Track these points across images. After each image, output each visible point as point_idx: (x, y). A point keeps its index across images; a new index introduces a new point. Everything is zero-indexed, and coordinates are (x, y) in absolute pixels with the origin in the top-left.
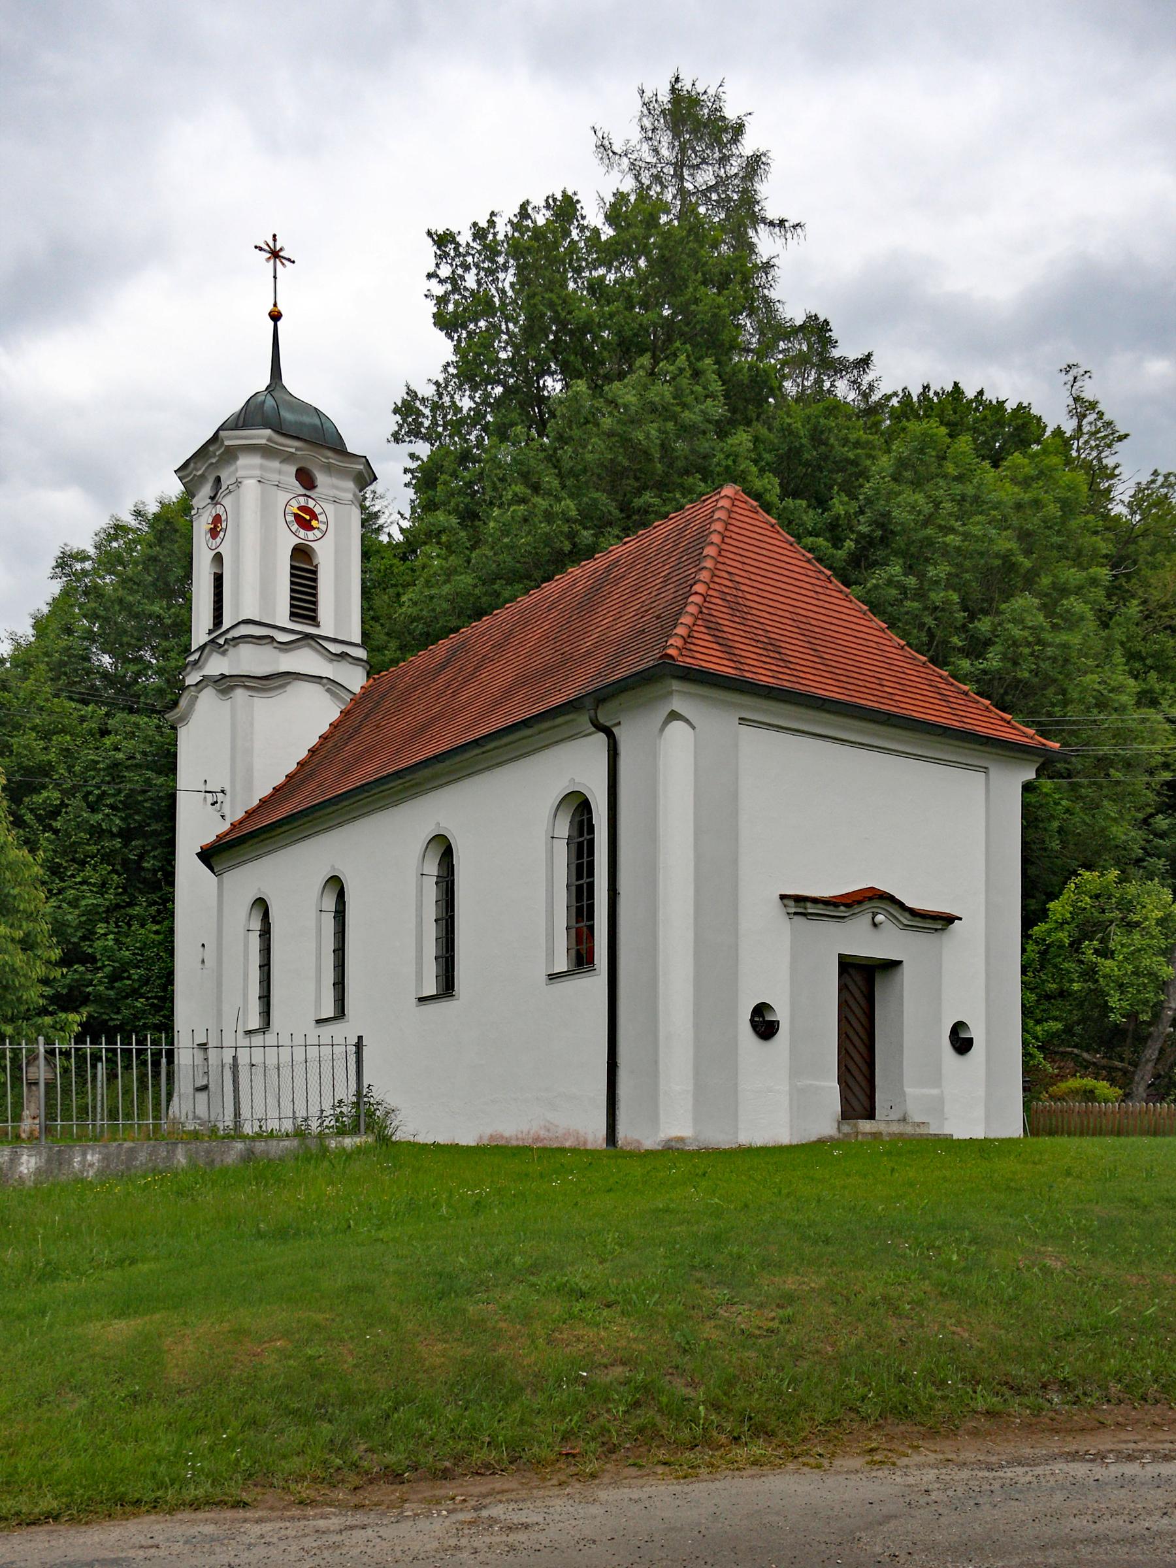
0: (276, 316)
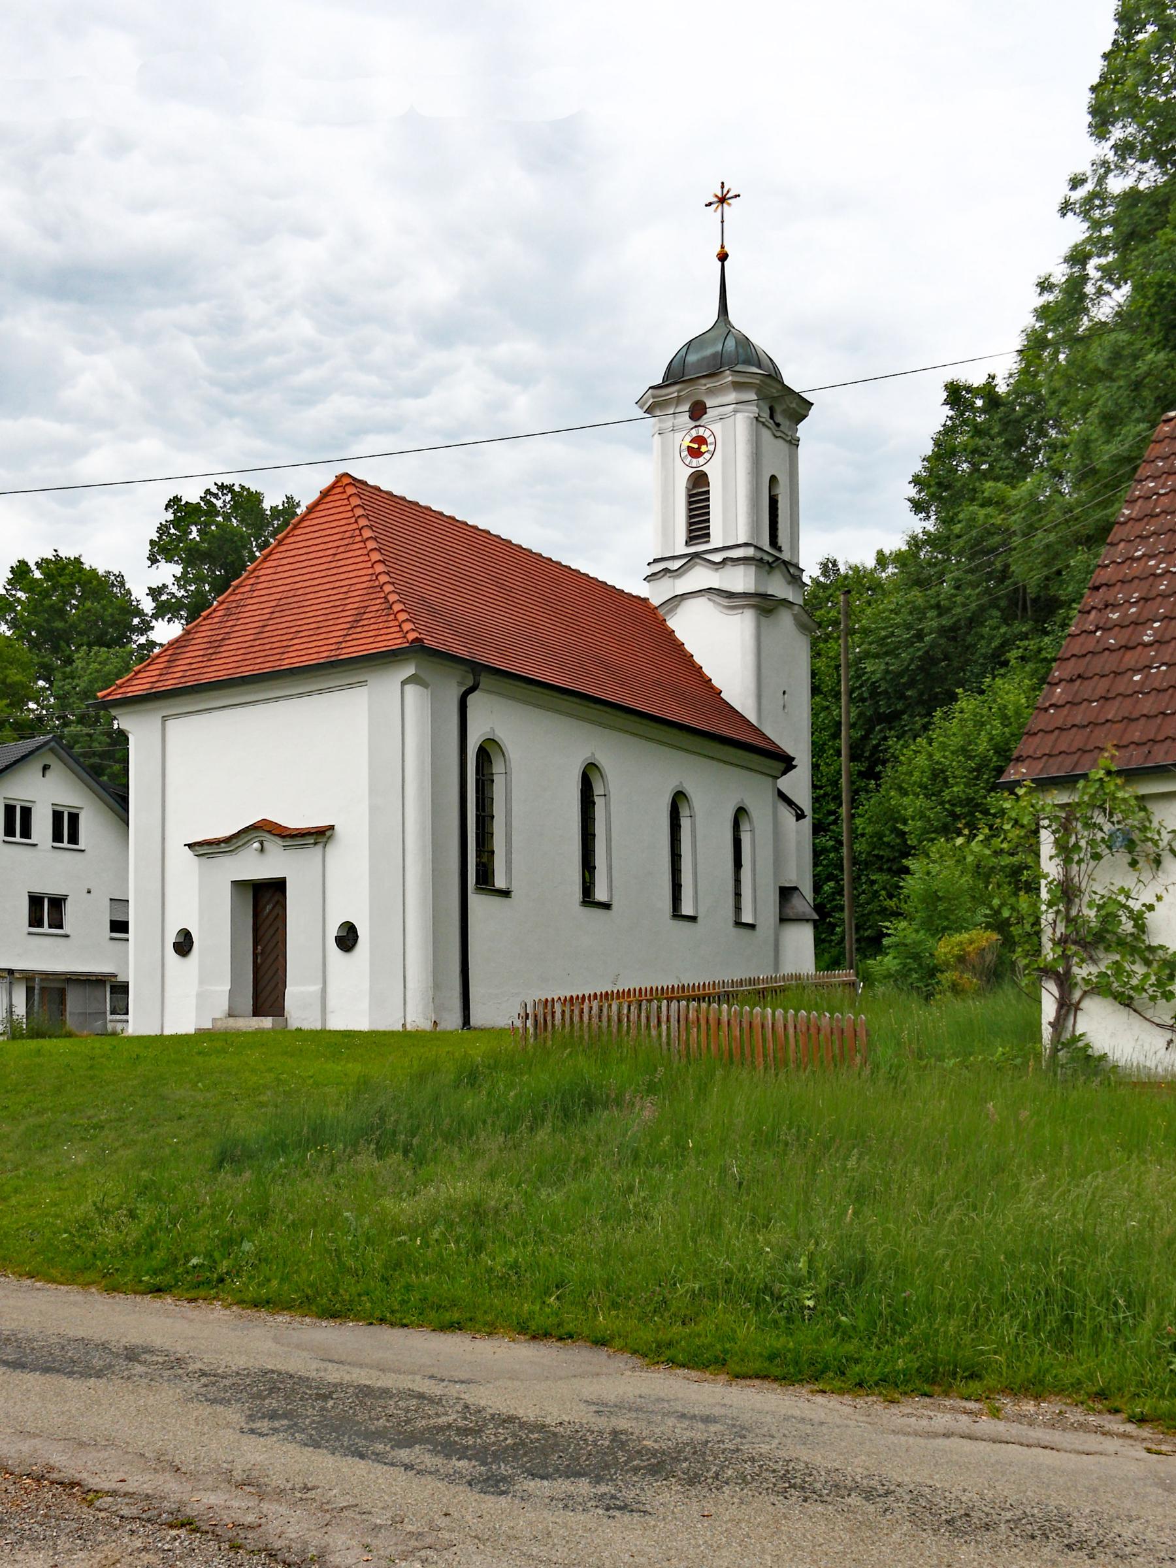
0: (723, 257)
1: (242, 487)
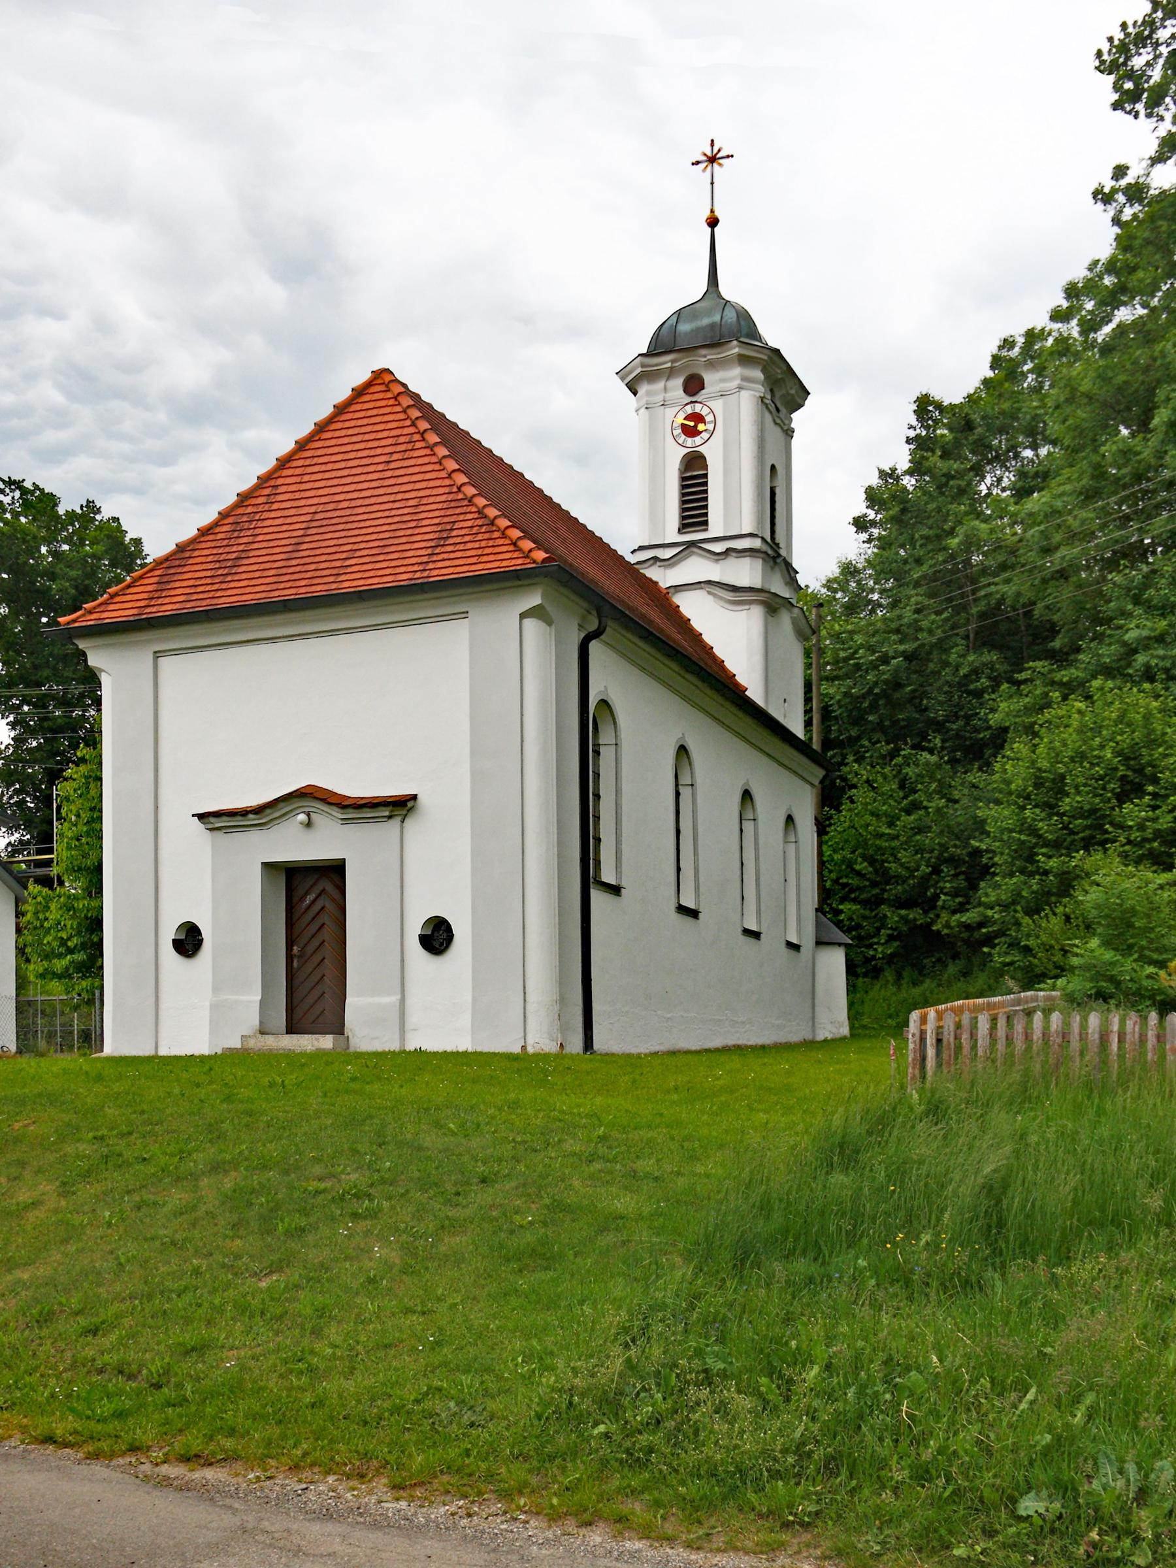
0: (713, 222)
1: (36, 487)
